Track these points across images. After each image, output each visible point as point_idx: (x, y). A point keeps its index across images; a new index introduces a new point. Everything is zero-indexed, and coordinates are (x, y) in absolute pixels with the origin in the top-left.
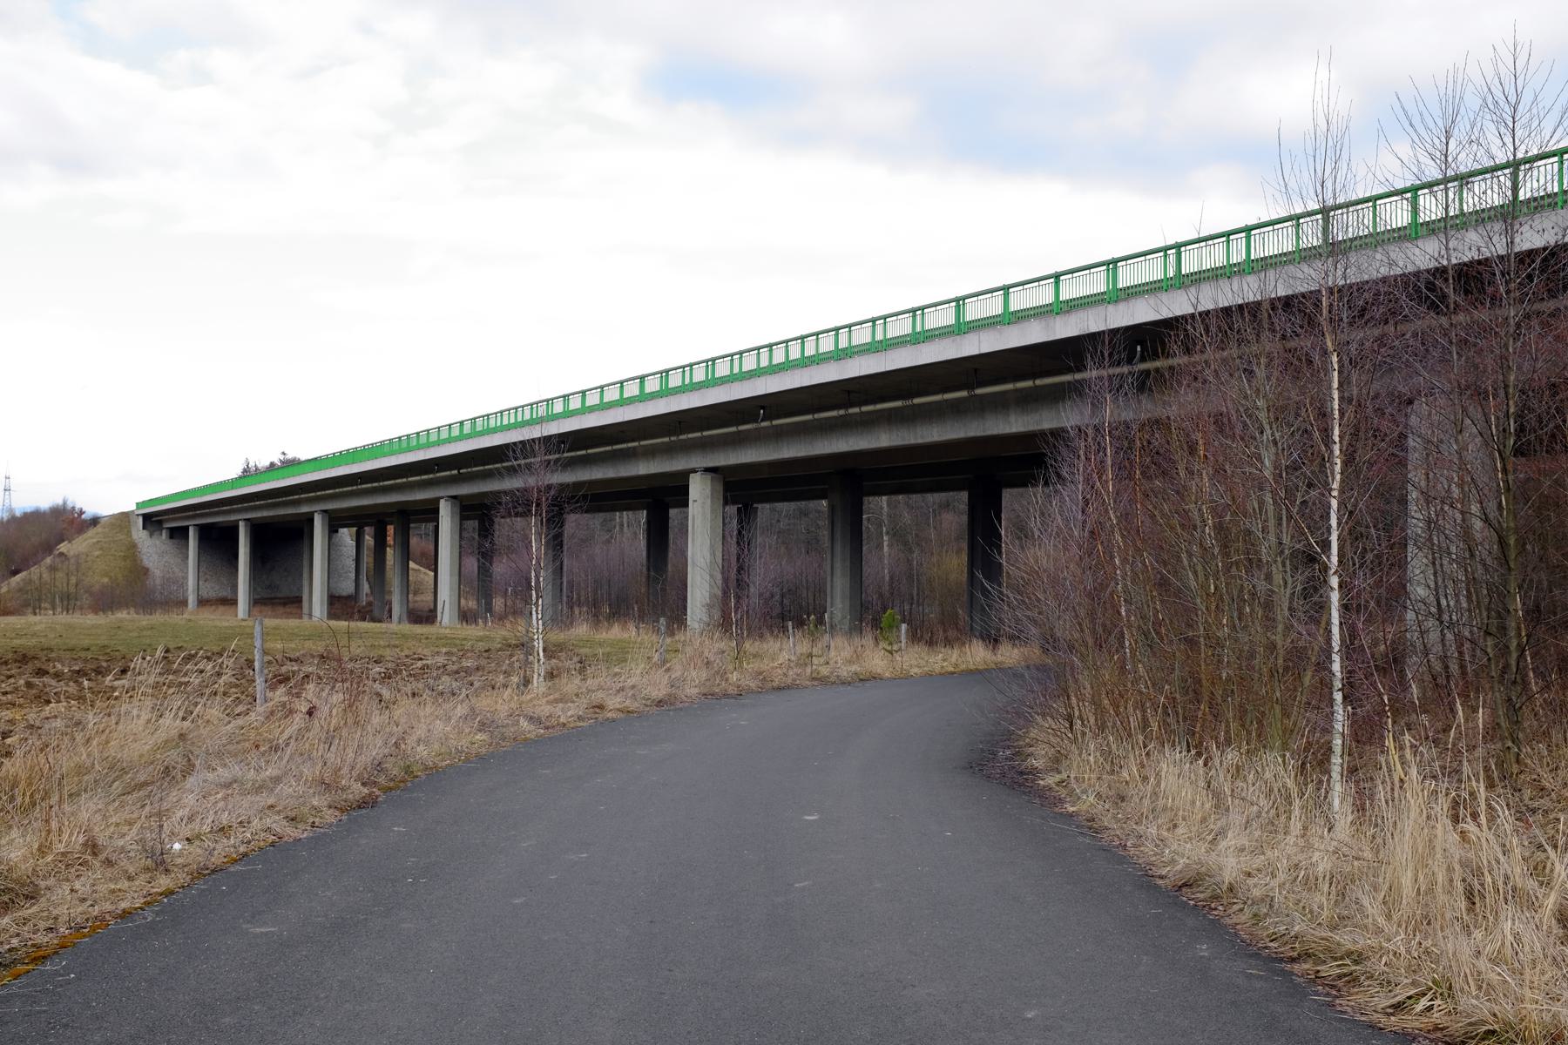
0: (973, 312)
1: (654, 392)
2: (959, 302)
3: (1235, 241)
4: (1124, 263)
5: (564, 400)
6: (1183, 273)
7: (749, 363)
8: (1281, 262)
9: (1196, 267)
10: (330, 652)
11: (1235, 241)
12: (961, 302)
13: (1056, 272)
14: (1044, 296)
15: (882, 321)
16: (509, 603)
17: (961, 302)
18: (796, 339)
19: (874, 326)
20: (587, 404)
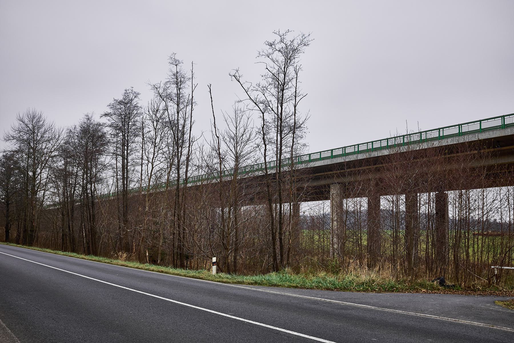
0: (348, 151)
1: (315, 159)
2: (503, 117)
3: (463, 127)
4: (334, 150)
5: (459, 127)
6: (422, 139)
7: (376, 145)
8: (463, 134)
9: (473, 129)
10: (262, 281)
11: (463, 127)
12: (460, 126)
13: (503, 115)
14: (476, 127)
15: (442, 130)
16: (134, 138)
17: (460, 126)
18: (385, 139)
19: (439, 131)
20: (321, 157)
